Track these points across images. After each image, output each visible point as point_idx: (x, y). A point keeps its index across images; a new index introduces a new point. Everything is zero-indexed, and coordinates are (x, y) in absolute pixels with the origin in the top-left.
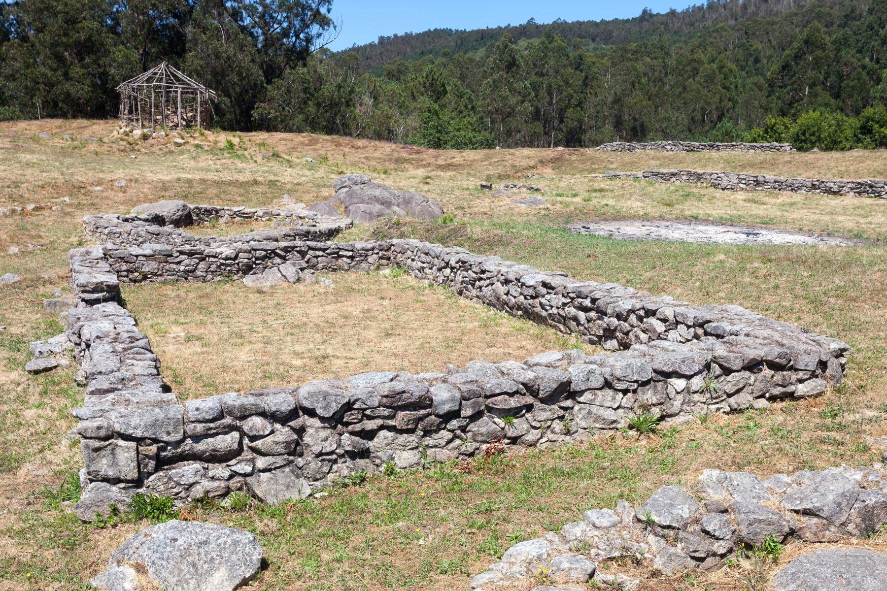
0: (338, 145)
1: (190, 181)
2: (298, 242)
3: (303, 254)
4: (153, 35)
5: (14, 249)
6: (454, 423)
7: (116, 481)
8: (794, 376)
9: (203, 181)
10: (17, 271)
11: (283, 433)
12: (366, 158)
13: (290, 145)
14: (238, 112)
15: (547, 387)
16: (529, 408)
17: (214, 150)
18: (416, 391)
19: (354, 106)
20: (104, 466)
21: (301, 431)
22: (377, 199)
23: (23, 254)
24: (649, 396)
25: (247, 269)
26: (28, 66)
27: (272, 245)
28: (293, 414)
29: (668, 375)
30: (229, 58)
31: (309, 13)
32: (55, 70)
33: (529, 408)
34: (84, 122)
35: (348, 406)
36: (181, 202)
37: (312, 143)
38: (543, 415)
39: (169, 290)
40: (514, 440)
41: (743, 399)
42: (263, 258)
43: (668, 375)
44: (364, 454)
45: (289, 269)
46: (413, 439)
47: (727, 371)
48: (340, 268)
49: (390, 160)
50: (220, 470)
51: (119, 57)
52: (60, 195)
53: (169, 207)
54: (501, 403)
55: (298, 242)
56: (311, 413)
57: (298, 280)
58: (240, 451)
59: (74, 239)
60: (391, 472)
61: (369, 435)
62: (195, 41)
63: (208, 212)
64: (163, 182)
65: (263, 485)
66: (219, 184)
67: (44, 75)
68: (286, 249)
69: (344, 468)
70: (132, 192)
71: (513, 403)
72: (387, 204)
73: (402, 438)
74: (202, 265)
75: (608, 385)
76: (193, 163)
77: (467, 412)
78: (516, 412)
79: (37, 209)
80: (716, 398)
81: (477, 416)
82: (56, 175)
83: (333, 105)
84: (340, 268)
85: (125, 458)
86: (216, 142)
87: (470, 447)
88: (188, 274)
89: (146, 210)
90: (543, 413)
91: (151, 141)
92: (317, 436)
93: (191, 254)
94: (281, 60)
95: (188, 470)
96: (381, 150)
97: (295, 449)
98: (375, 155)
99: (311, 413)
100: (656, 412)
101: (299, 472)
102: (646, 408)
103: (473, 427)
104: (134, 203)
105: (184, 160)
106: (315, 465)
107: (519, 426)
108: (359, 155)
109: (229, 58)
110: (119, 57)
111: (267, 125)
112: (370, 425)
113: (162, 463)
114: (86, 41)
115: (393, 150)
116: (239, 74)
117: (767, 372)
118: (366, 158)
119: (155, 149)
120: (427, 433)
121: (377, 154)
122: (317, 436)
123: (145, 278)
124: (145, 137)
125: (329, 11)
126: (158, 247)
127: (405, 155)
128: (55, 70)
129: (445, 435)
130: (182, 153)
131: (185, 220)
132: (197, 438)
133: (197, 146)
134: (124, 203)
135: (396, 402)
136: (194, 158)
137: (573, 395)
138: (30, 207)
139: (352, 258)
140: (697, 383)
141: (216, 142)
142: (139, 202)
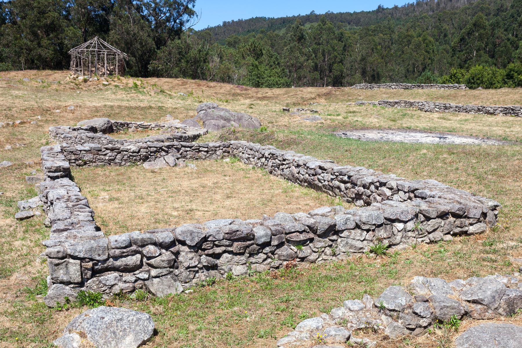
0: (199, 85)
1: (112, 107)
2: (175, 143)
3: (178, 150)
4: (90, 20)
5: (8, 147)
6: (267, 249)
7: (68, 283)
8: (467, 222)
9: (119, 107)
10: (10, 159)
11: (167, 255)
12: (216, 93)
13: (171, 85)
14: (140, 66)
15: (322, 228)
16: (311, 240)
17: (126, 88)
18: (245, 230)
19: (208, 62)
20: (61, 274)
21: (177, 254)
22: (222, 117)
23: (14, 149)
24: (382, 233)
25: (146, 159)
26: (16, 39)
27: (160, 144)
28: (173, 244)
29: (393, 221)
30: (135, 34)
31: (182, 8)
32: (32, 41)
33: (311, 240)
34: (49, 72)
35: (205, 239)
36: (106, 119)
37: (183, 84)
38: (320, 245)
39: (99, 171)
40: (303, 259)
41: (437, 235)
42: (155, 152)
43: (393, 221)
44: (214, 267)
45: (170, 159)
46: (243, 258)
47: (428, 219)
48: (200, 158)
49: (229, 94)
50: (129, 277)
51: (70, 33)
52: (35, 115)
53: (99, 122)
54: (295, 237)
55: (175, 143)
56: (183, 243)
57: (176, 165)
58: (141, 265)
59: (44, 141)
60: (230, 278)
61: (217, 256)
62: (115, 24)
63: (122, 125)
64: (96, 107)
65: (155, 285)
66: (129, 108)
67: (26, 44)
68: (168, 147)
69: (202, 275)
70: (78, 113)
71: (302, 237)
72: (228, 120)
73: (237, 258)
74: (119, 156)
75: (358, 226)
76: (113, 96)
77: (275, 242)
78: (303, 243)
79: (22, 123)
80: (421, 234)
81: (280, 245)
82: (33, 103)
83: (196, 62)
84: (200, 158)
85: (74, 270)
86: (127, 84)
87: (276, 263)
88: (111, 161)
89: (86, 124)
90: (320, 243)
91: (89, 83)
92: (187, 257)
93: (112, 150)
94: (165, 35)
95: (111, 277)
96: (224, 88)
97: (173, 264)
98: (221, 91)
99: (183, 243)
100: (386, 243)
101: (176, 278)
102: (380, 240)
103: (278, 251)
104: (79, 119)
105: (108, 94)
106: (185, 274)
107: (306, 251)
108: (211, 91)
109: (135, 34)
110: (70, 33)
111: (157, 74)
112: (218, 250)
113: (95, 273)
114: (51, 24)
115: (232, 88)
116: (141, 43)
117: (451, 219)
118: (216, 93)
119: (91, 88)
120: (251, 255)
121: (222, 91)
122: (187, 257)
123: (85, 163)
124: (85, 81)
125: (194, 6)
126: (93, 145)
127: (238, 91)
128: (32, 41)
129: (262, 256)
130: (107, 90)
131: (109, 130)
132: (116, 258)
133: (116, 86)
134: (73, 119)
135: (233, 237)
136: (114, 93)
137: (337, 233)
138: (18, 122)
139: (207, 152)
140: (410, 225)
141: (127, 84)
142: (82, 119)
